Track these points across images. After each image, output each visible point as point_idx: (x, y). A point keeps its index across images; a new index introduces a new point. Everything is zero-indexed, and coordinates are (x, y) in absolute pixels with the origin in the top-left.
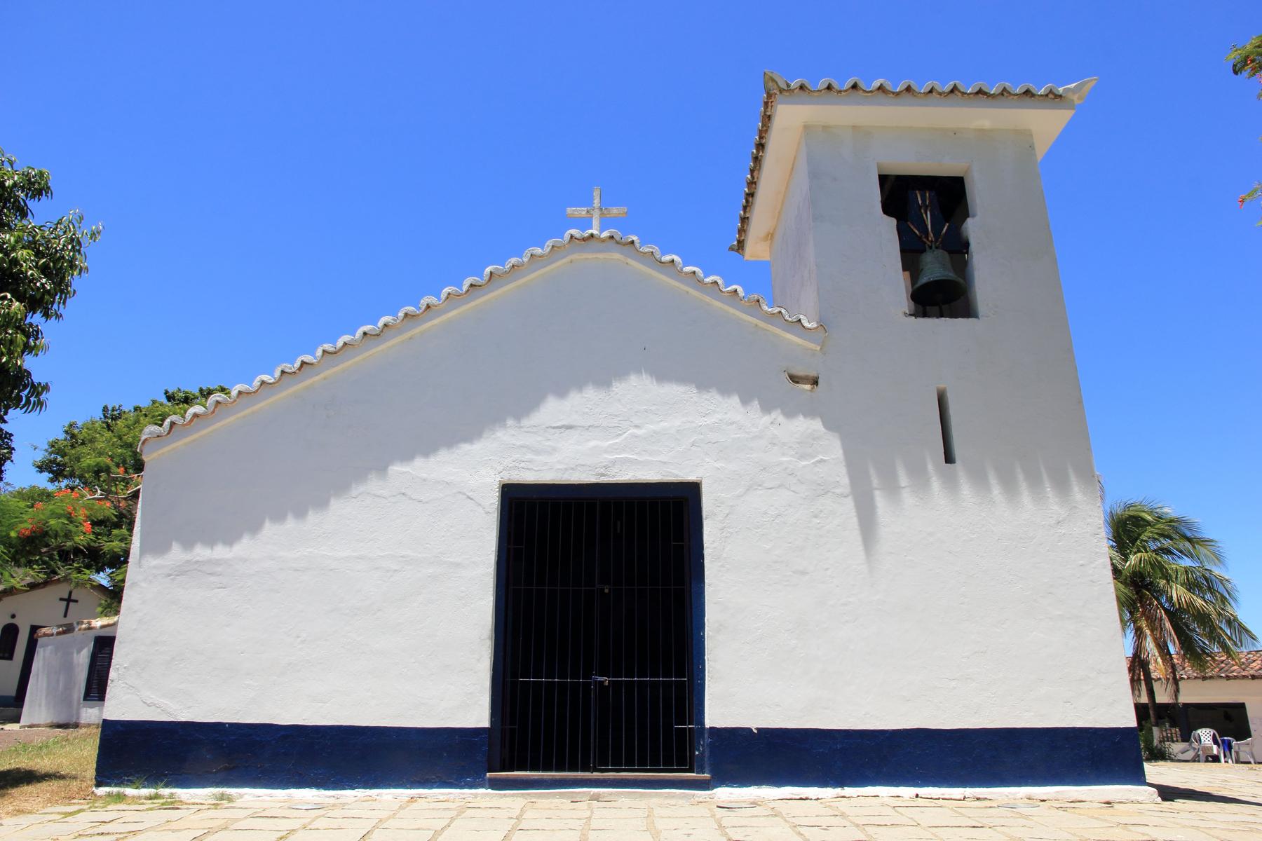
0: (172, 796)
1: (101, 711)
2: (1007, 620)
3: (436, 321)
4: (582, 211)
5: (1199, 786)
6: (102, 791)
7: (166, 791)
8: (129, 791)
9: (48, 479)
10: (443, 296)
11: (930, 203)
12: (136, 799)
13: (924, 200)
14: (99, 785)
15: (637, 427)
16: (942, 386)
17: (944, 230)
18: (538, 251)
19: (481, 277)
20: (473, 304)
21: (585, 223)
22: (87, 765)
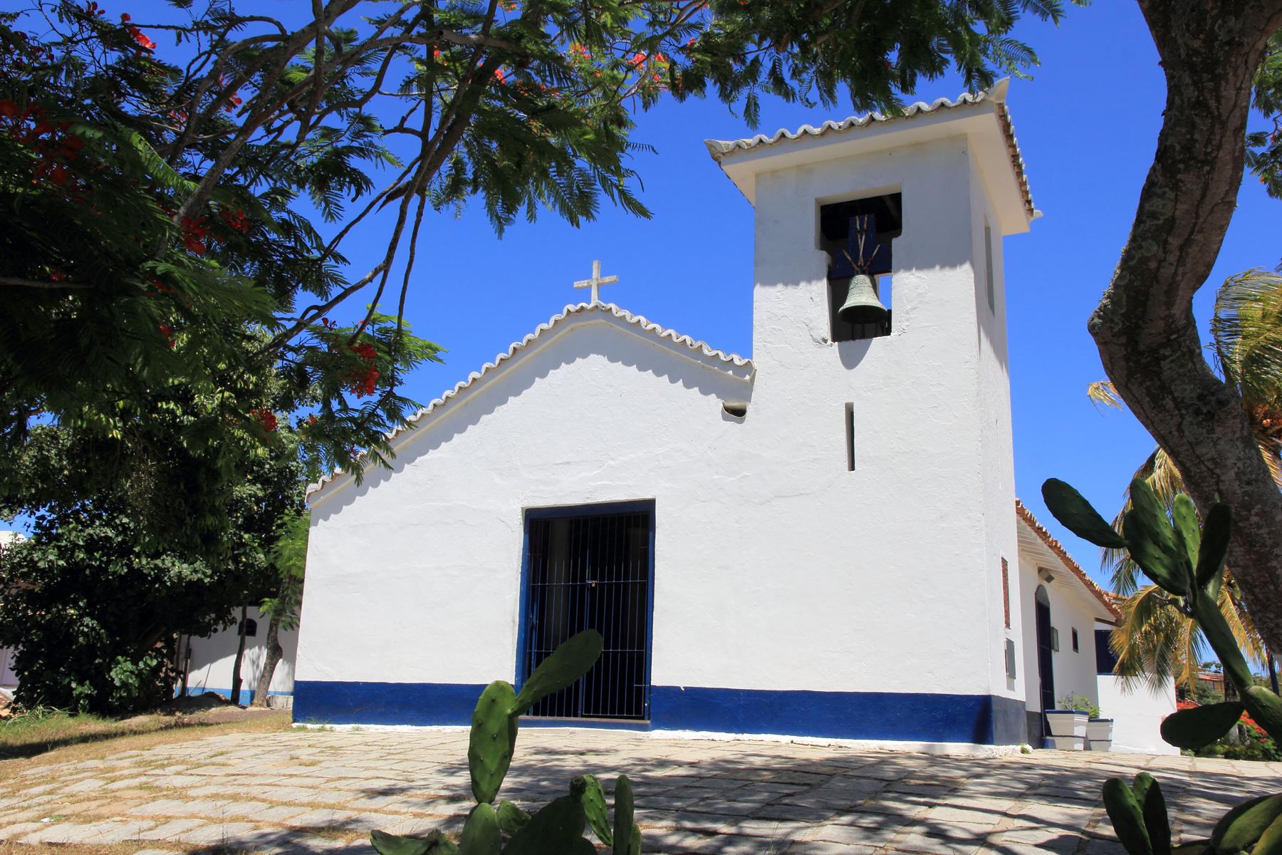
0: (331, 728)
1: (293, 671)
2: (494, 739)
3: (482, 389)
4: (584, 283)
5: (965, 805)
6: (295, 725)
7: (328, 726)
8: (309, 726)
9: (833, 350)
10: (483, 370)
11: (867, 226)
12: (312, 730)
13: (861, 225)
14: (295, 721)
15: (613, 459)
16: (850, 401)
17: (849, 258)
18: (545, 326)
19: (507, 353)
20: (505, 373)
21: (585, 294)
22: (1172, 419)
